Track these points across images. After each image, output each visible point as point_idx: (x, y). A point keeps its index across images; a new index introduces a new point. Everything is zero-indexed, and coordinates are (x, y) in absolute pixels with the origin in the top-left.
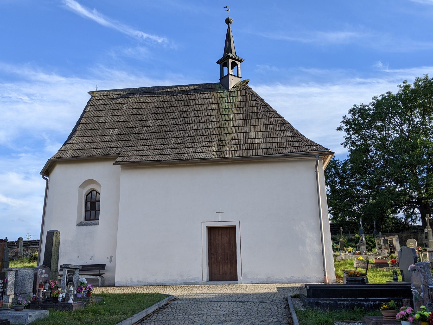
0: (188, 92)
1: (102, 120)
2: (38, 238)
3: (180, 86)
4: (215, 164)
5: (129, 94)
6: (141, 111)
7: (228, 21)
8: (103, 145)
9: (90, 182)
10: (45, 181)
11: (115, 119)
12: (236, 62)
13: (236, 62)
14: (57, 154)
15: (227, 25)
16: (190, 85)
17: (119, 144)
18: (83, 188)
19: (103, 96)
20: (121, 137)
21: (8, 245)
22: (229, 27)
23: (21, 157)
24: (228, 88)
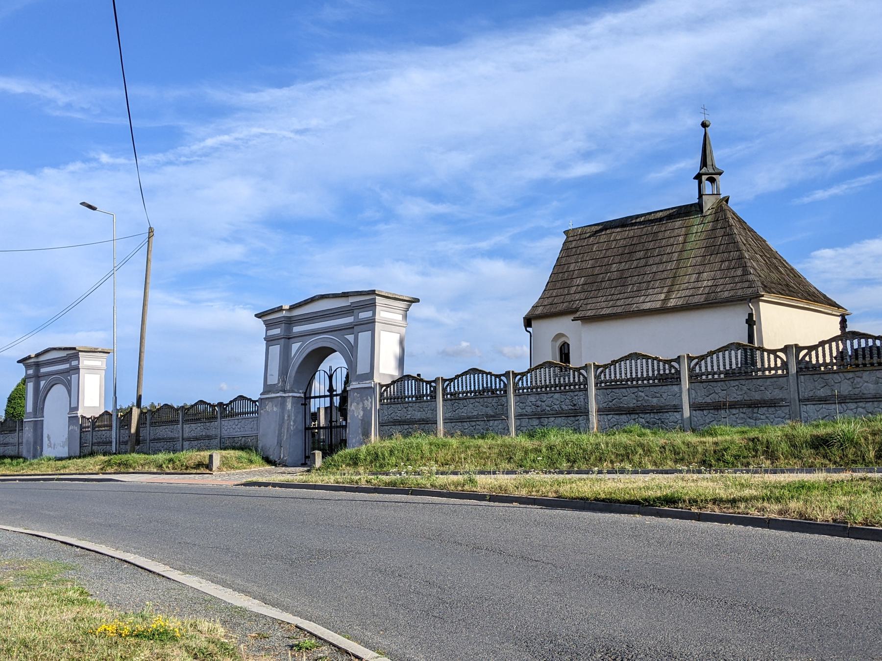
0: (661, 219)
1: (572, 267)
2: (98, 405)
3: (651, 213)
4: (659, 313)
5: (601, 230)
6: (609, 253)
7: (704, 125)
8: (568, 298)
9: (560, 335)
10: (529, 334)
11: (584, 265)
12: (713, 176)
13: (713, 176)
14: (529, 312)
15: (704, 129)
16: (669, 209)
17: (582, 296)
18: (556, 342)
19: (577, 236)
20: (586, 287)
21: (599, 413)
22: (705, 130)
23: (587, 156)
24: (702, 211)
